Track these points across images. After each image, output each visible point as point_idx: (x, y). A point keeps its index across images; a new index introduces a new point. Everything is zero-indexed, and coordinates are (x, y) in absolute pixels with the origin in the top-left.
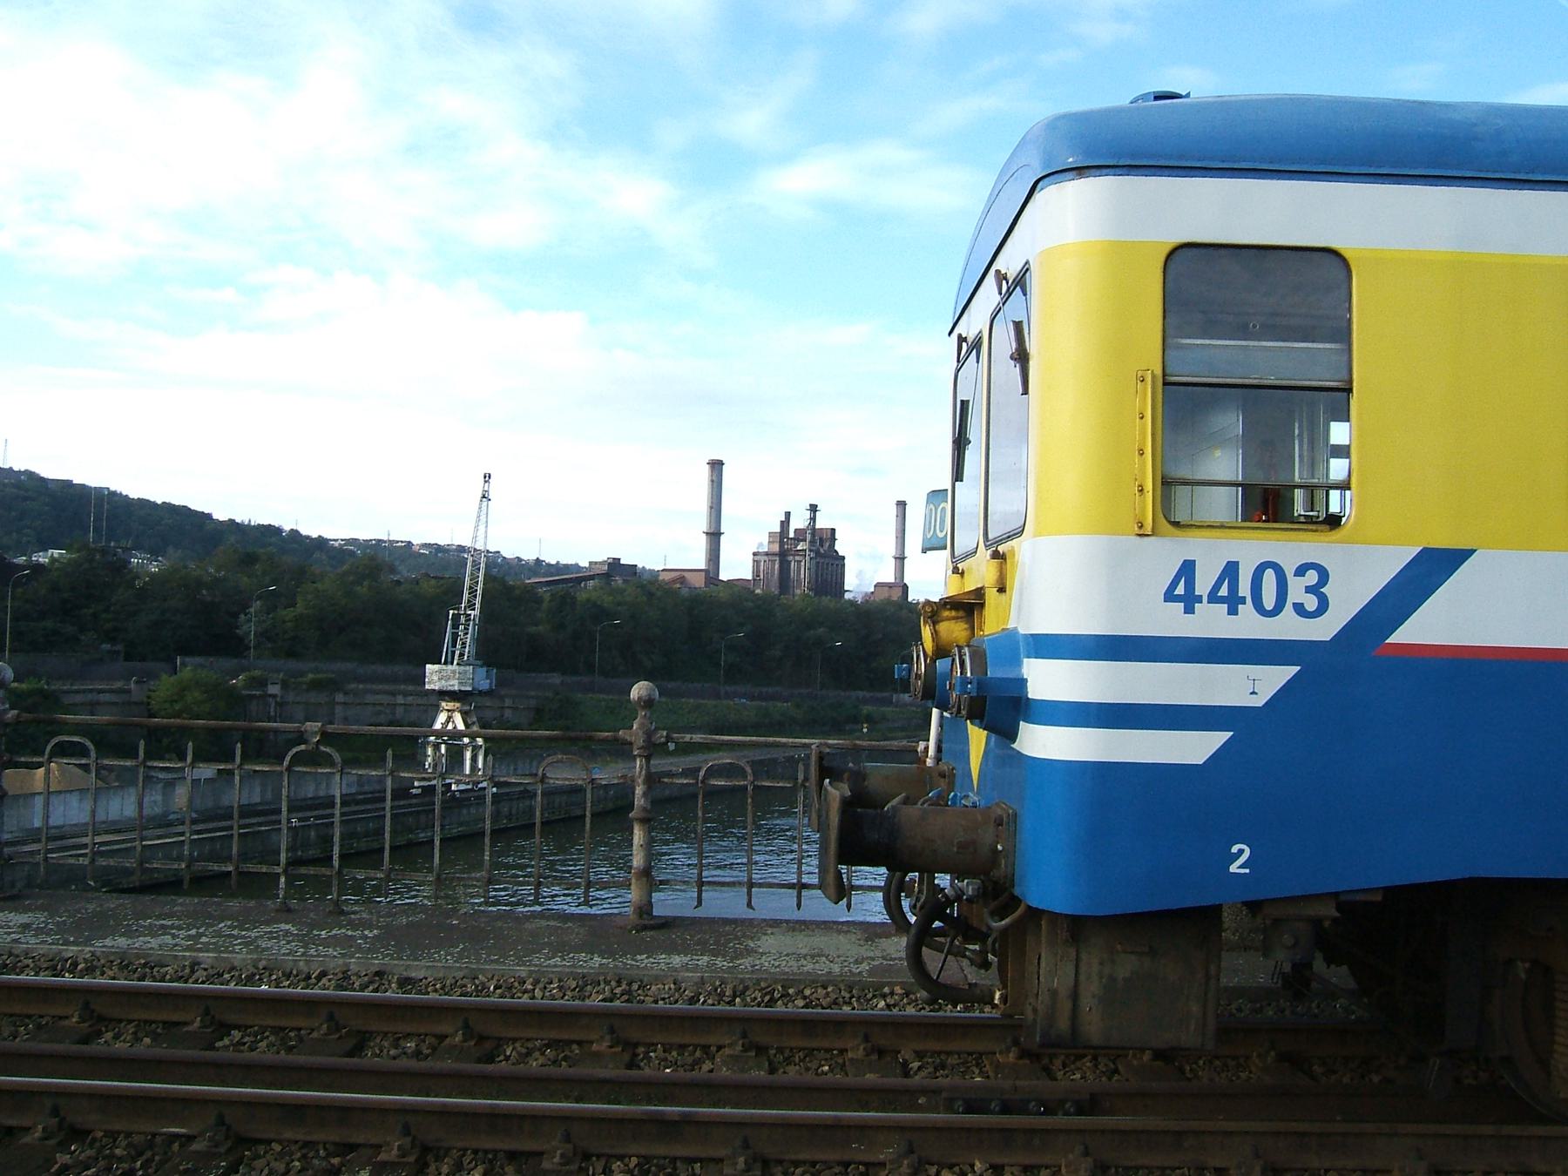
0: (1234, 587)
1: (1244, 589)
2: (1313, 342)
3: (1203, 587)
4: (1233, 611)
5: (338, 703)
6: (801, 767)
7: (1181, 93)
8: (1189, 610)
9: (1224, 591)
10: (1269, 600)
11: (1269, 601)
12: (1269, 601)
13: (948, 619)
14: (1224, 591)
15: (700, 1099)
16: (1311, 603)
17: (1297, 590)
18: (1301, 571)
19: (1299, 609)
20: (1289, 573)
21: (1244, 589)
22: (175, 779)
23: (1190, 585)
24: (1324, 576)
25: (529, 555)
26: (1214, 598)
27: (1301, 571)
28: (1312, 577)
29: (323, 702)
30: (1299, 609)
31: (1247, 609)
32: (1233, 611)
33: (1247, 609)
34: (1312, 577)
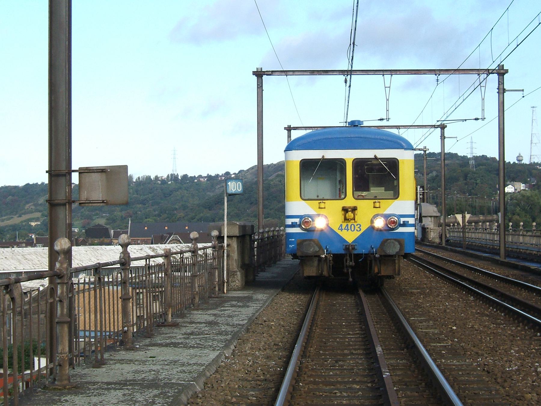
0: (348, 227)
1: (349, 228)
2: (224, 215)
3: (343, 228)
4: (348, 231)
5: (92, 331)
6: (141, 295)
7: (413, 144)
8: (341, 231)
9: (346, 228)
10: (353, 229)
11: (353, 230)
12: (353, 230)
13: (114, 263)
14: (346, 228)
15: (495, 343)
16: (359, 229)
17: (357, 228)
18: (357, 225)
19: (357, 230)
20: (355, 225)
21: (349, 228)
22: (226, 193)
23: (342, 228)
24: (360, 226)
25: (163, 174)
26: (345, 229)
27: (357, 225)
28: (359, 226)
29: (177, 207)
30: (357, 230)
31: (350, 230)
32: (348, 231)
33: (350, 230)
34: (359, 226)
